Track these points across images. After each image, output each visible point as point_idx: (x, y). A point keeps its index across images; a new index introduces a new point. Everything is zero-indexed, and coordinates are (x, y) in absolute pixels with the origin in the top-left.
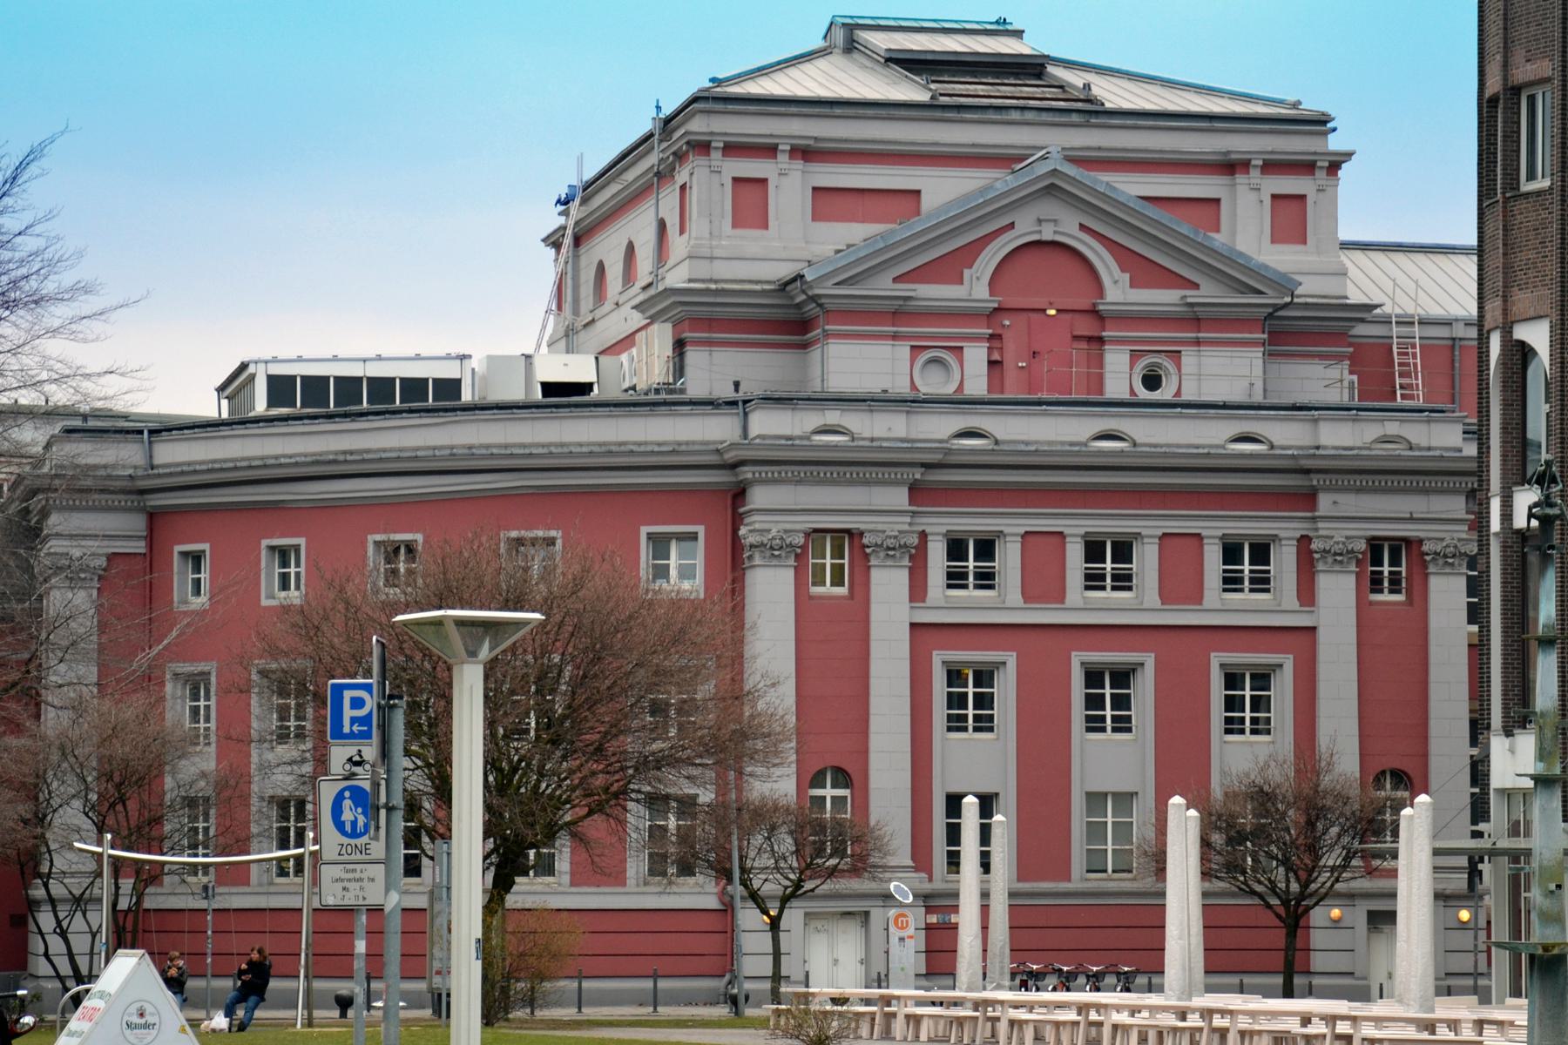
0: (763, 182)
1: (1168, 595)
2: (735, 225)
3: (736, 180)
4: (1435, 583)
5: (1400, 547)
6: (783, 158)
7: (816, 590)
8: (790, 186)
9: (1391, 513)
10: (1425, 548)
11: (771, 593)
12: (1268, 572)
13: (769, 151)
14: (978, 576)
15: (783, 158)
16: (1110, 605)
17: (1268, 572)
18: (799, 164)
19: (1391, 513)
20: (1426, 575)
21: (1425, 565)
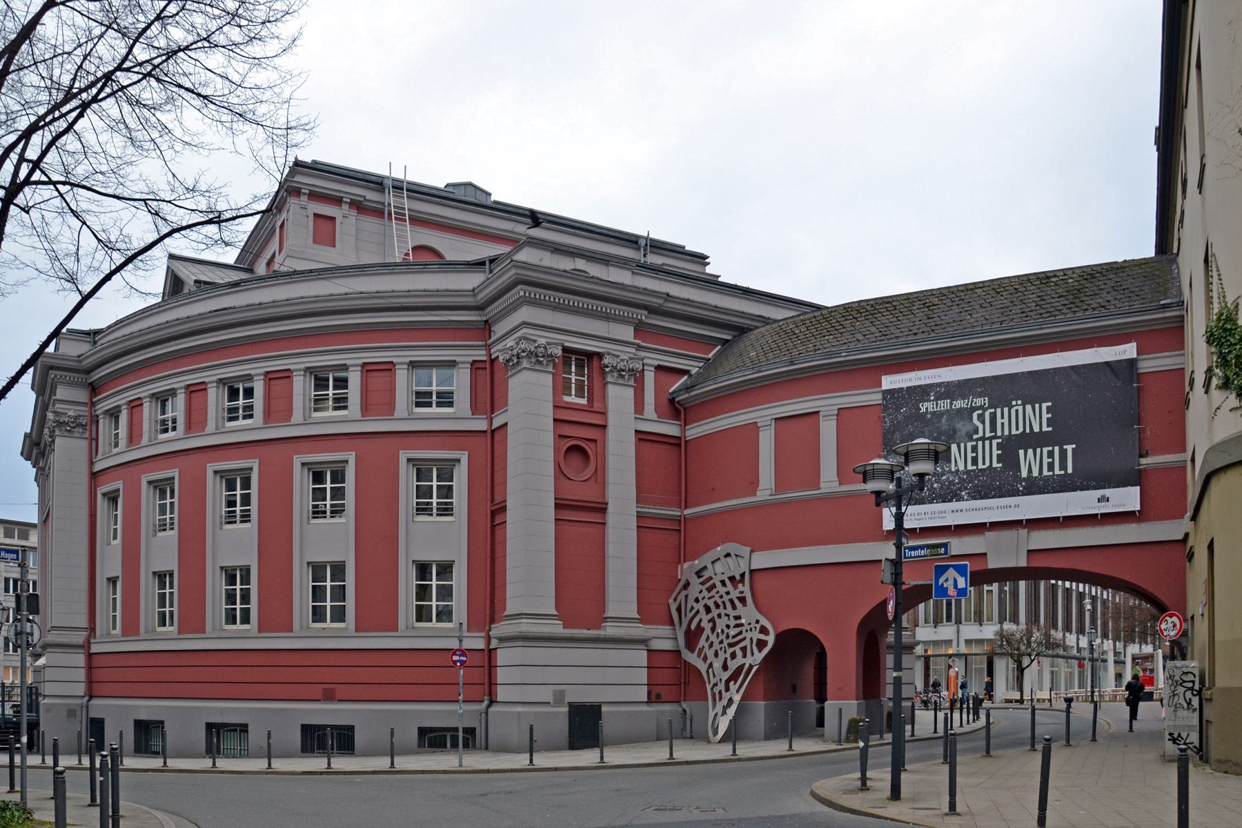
0: (333, 219)
1: (366, 408)
2: (315, 242)
3: (316, 215)
4: (612, 390)
5: (588, 359)
6: (345, 207)
7: (566, 399)
8: (347, 221)
9: (587, 331)
10: (606, 361)
11: (531, 399)
12: (451, 503)
13: (337, 201)
14: (336, 400)
15: (345, 207)
16: (330, 420)
17: (451, 503)
18: (354, 212)
19: (587, 331)
20: (605, 384)
21: (603, 374)
